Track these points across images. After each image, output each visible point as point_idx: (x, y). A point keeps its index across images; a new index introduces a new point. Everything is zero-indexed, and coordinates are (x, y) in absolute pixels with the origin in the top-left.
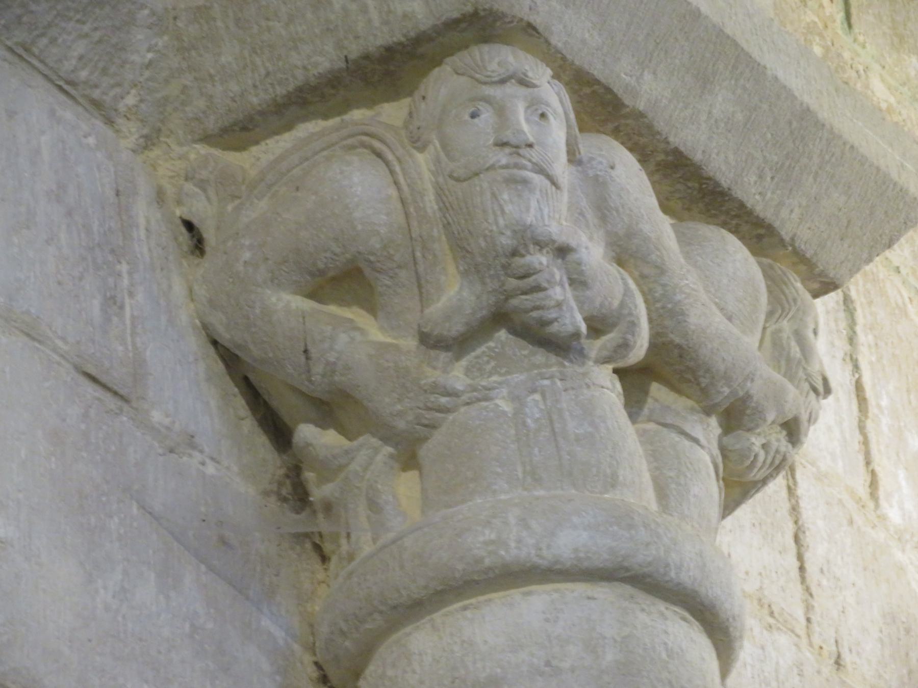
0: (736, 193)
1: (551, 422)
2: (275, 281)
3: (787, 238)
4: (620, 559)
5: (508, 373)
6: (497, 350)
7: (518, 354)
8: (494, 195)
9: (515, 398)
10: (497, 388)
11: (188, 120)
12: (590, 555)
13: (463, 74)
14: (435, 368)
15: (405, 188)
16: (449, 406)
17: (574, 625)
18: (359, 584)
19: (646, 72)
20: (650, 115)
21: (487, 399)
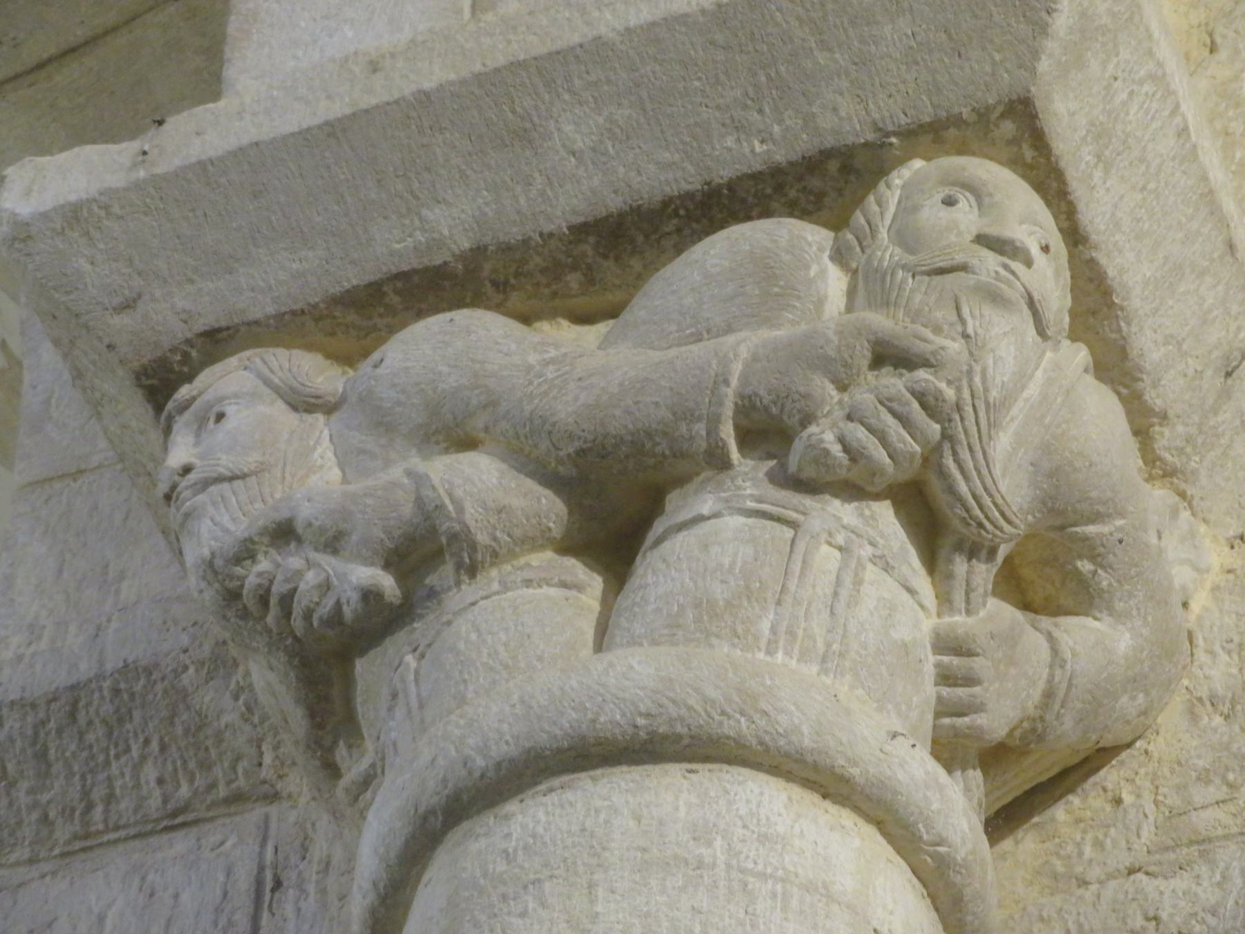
0: (722, 178)
3: (870, 136)
19: (425, 212)
20: (487, 239)
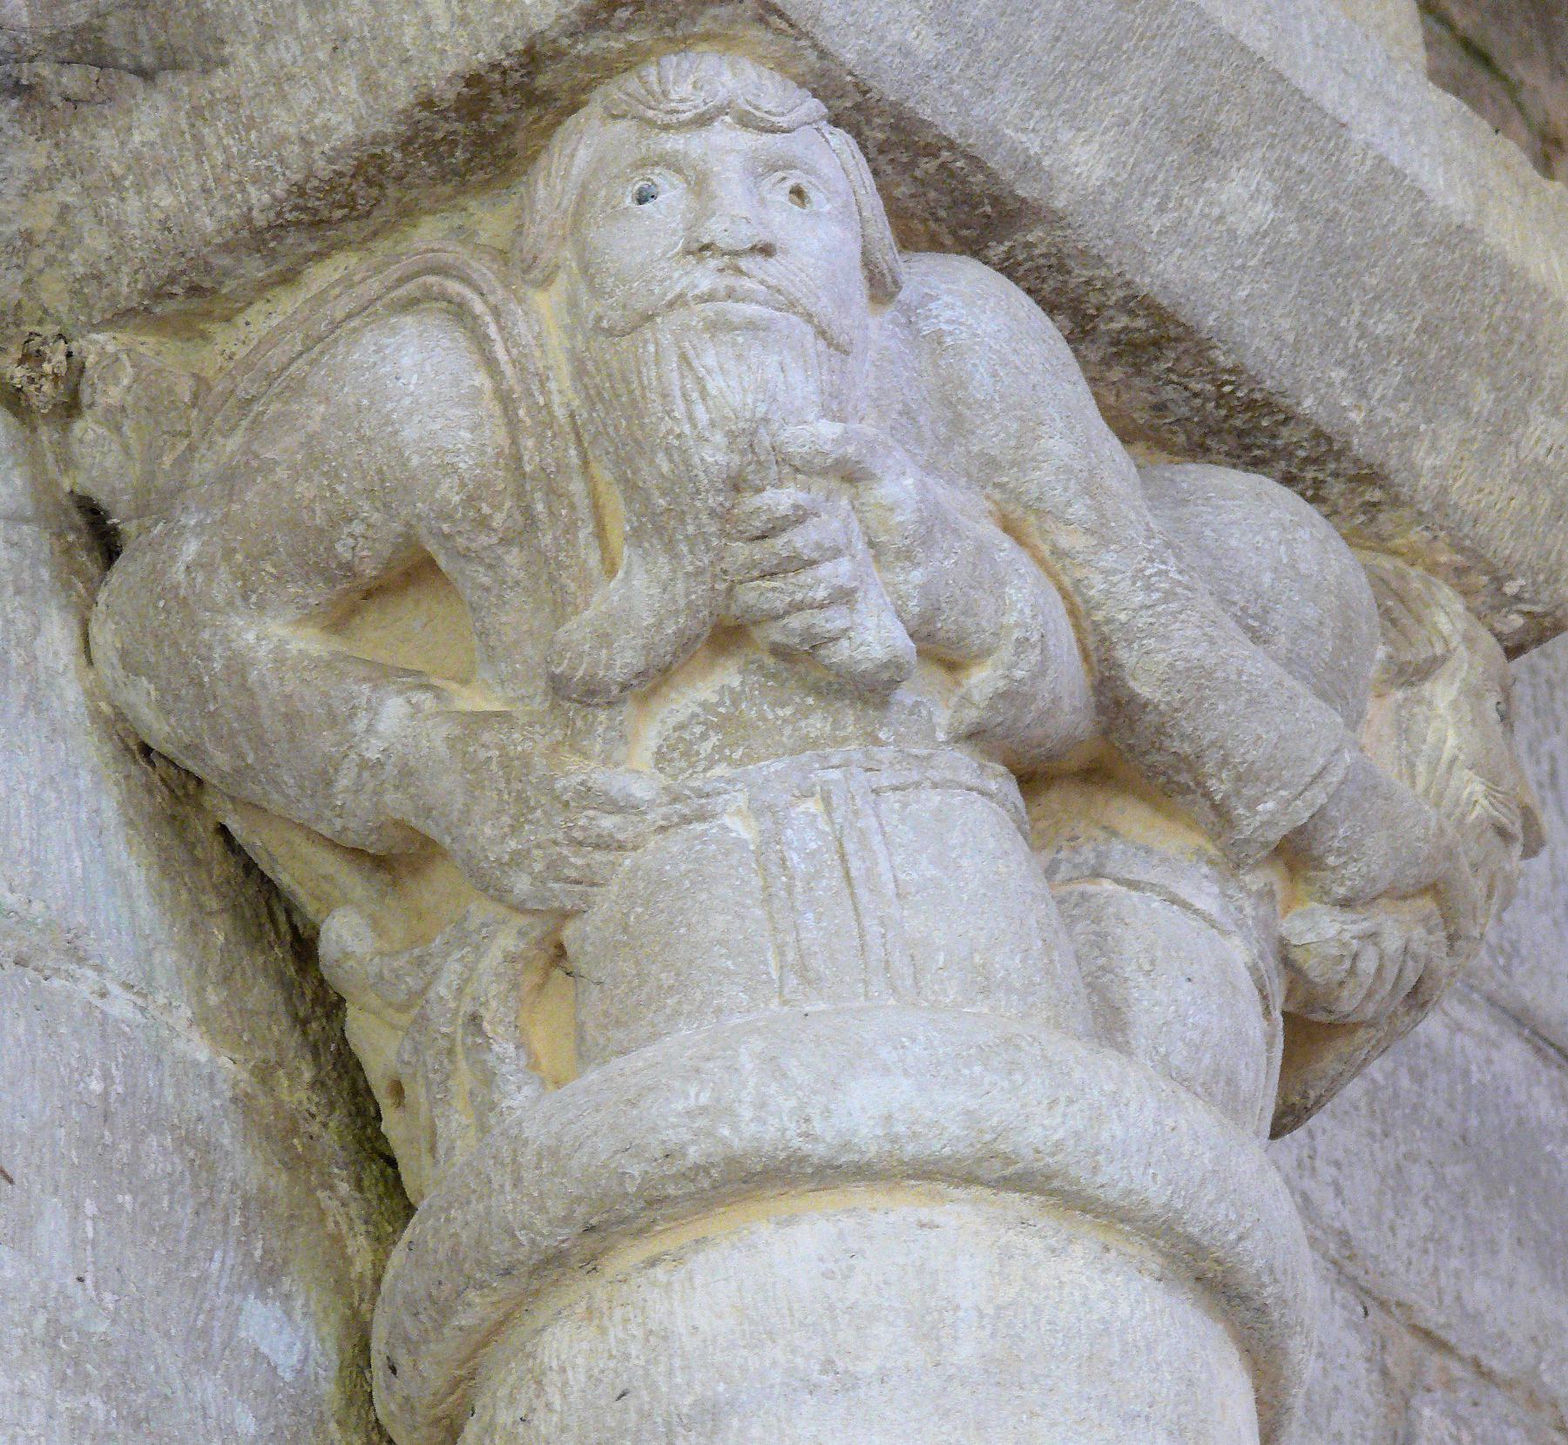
1: (843, 858)
2: (248, 593)
4: (988, 1137)
5: (748, 758)
6: (722, 710)
7: (771, 716)
8: (684, 358)
9: (760, 810)
10: (726, 792)
11: (77, 280)
12: (918, 1128)
13: (623, 116)
14: (585, 755)
15: (508, 369)
16: (620, 836)
17: (886, 1283)
18: (436, 1231)
21: (702, 817)
